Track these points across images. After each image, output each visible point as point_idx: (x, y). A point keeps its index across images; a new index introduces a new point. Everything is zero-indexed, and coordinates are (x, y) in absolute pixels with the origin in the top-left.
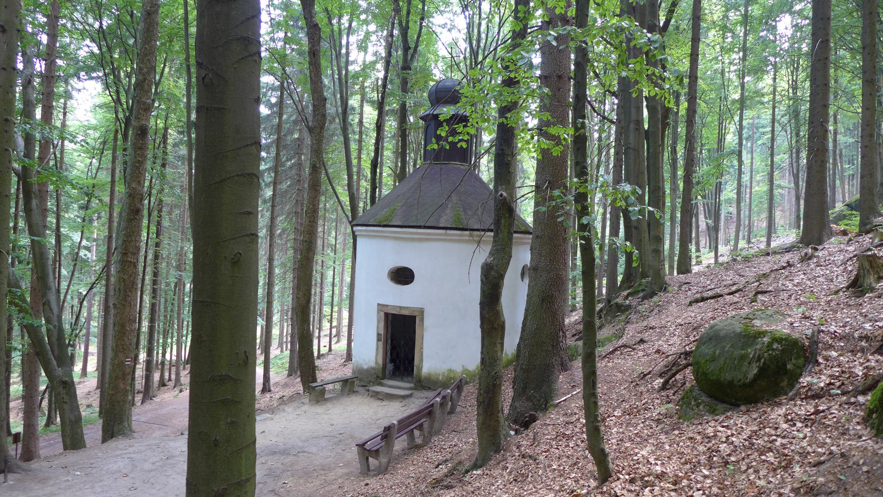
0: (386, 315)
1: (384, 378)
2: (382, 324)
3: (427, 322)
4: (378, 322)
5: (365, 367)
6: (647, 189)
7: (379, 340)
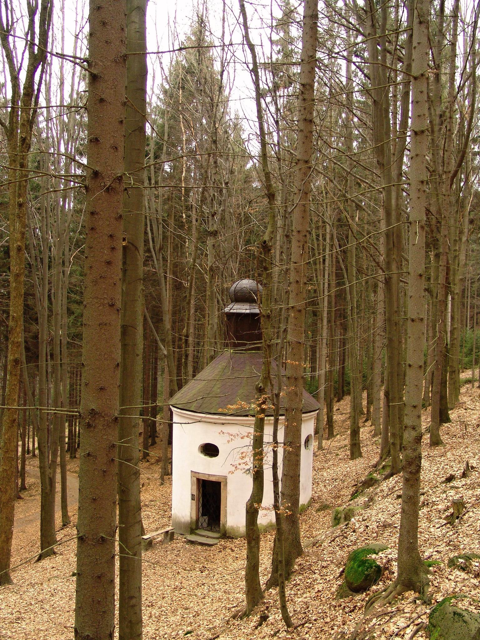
0: (198, 480)
1: (197, 528)
2: (195, 487)
3: (230, 487)
4: (192, 486)
5: (183, 520)
6: (118, 512)
7: (193, 499)
